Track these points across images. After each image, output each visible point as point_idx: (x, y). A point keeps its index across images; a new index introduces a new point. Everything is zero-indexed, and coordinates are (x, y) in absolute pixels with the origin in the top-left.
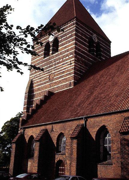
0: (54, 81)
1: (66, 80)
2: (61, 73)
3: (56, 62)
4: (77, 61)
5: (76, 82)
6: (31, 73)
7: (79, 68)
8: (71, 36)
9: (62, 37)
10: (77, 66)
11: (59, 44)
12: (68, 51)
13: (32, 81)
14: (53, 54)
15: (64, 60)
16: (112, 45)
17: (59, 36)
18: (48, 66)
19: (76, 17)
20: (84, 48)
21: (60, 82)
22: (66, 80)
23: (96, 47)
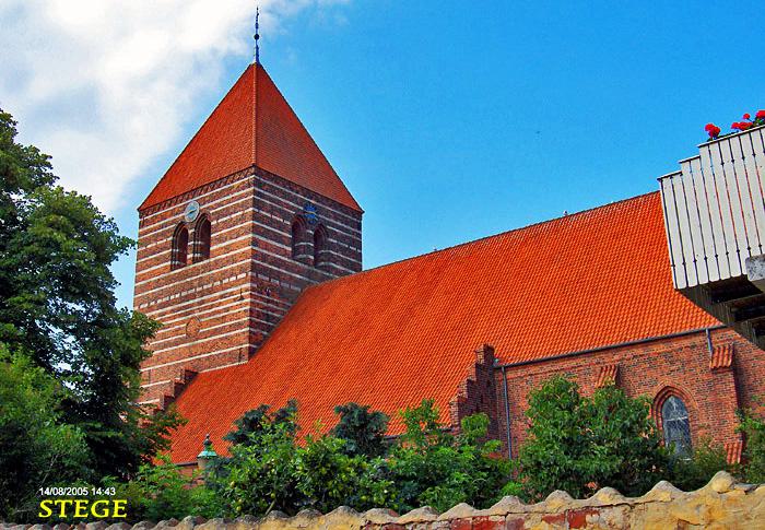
1: (229, 341)
2: (218, 319)
3: (205, 287)
4: (259, 289)
5: (255, 349)
7: (265, 308)
8: (242, 219)
9: (219, 215)
11: (211, 249)
12: (233, 260)
14: (195, 260)
18: (183, 294)
19: (254, 165)
20: (277, 250)
21: (214, 345)
22: (229, 341)
23: (316, 238)
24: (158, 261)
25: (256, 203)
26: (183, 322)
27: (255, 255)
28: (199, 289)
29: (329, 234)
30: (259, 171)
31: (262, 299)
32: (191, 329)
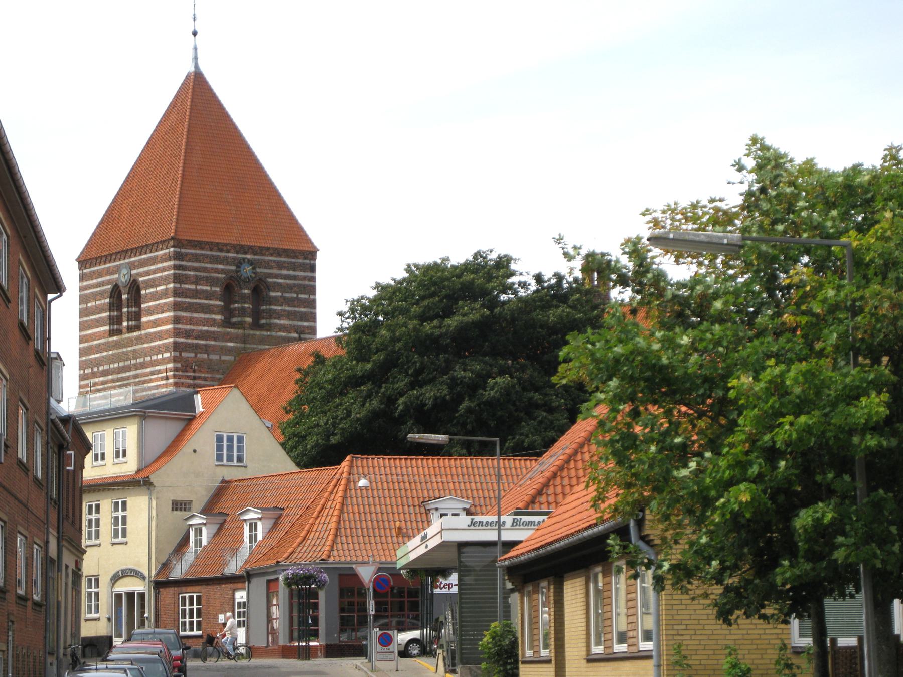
16: (321, 262)
17: (141, 279)
18: (121, 364)
19: (172, 238)
23: (256, 291)
25: (177, 279)
27: (177, 333)
28: (133, 362)
29: (270, 287)
30: (177, 242)
31: (188, 377)
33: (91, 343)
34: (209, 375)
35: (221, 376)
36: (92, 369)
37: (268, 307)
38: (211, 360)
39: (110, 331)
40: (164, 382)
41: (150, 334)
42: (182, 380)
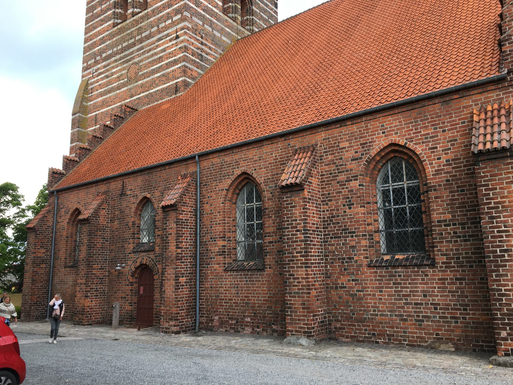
0: (140, 82)
3: (144, 35)
6: (85, 65)
7: (198, 48)
10: (193, 44)
13: (87, 85)
14: (134, 14)
15: (162, 28)
18: (124, 45)
24: (103, 21)
26: (124, 69)
32: (132, 74)
33: (95, 40)
34: (213, 47)
35: (222, 52)
36: (95, 59)
37: (251, 17)
38: (215, 35)
39: (114, 24)
40: (174, 42)
41: (158, 8)
42: (192, 40)
